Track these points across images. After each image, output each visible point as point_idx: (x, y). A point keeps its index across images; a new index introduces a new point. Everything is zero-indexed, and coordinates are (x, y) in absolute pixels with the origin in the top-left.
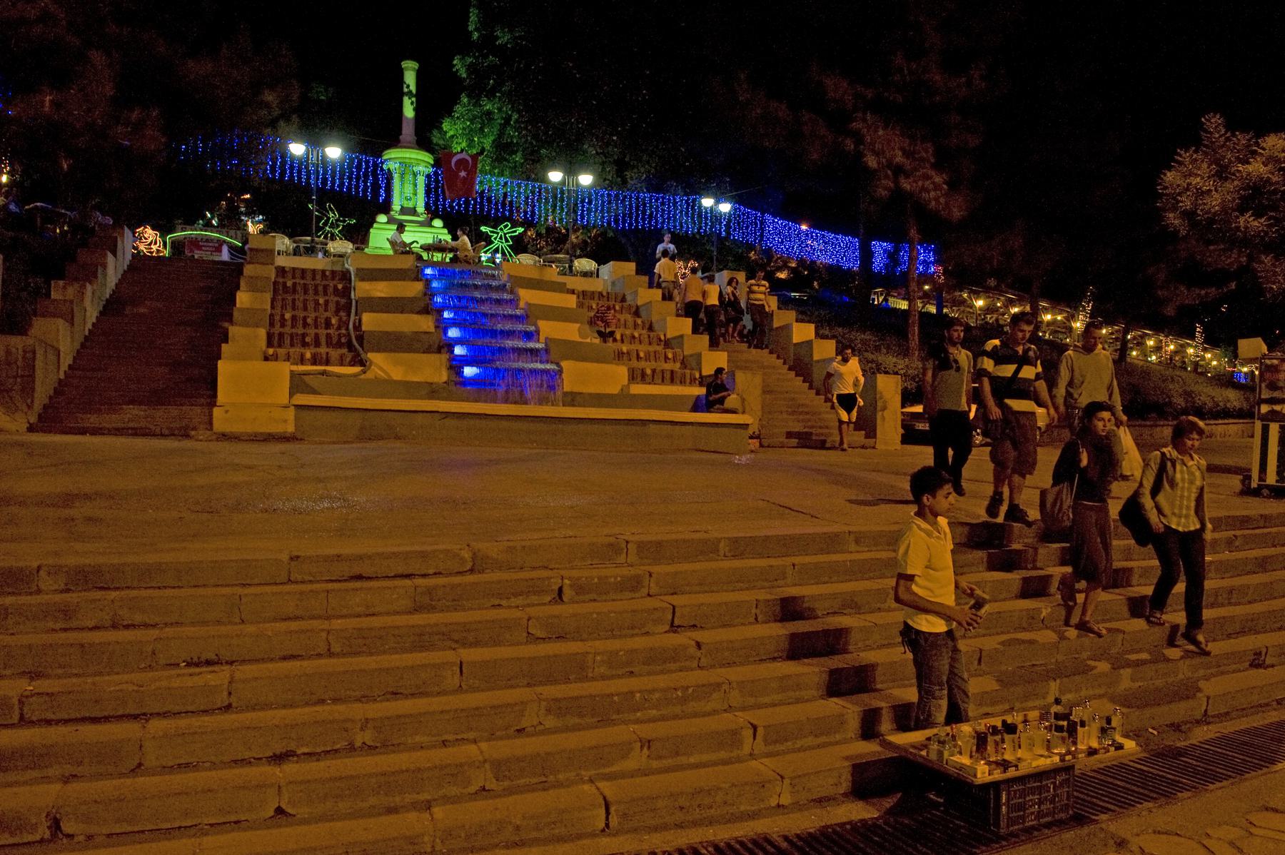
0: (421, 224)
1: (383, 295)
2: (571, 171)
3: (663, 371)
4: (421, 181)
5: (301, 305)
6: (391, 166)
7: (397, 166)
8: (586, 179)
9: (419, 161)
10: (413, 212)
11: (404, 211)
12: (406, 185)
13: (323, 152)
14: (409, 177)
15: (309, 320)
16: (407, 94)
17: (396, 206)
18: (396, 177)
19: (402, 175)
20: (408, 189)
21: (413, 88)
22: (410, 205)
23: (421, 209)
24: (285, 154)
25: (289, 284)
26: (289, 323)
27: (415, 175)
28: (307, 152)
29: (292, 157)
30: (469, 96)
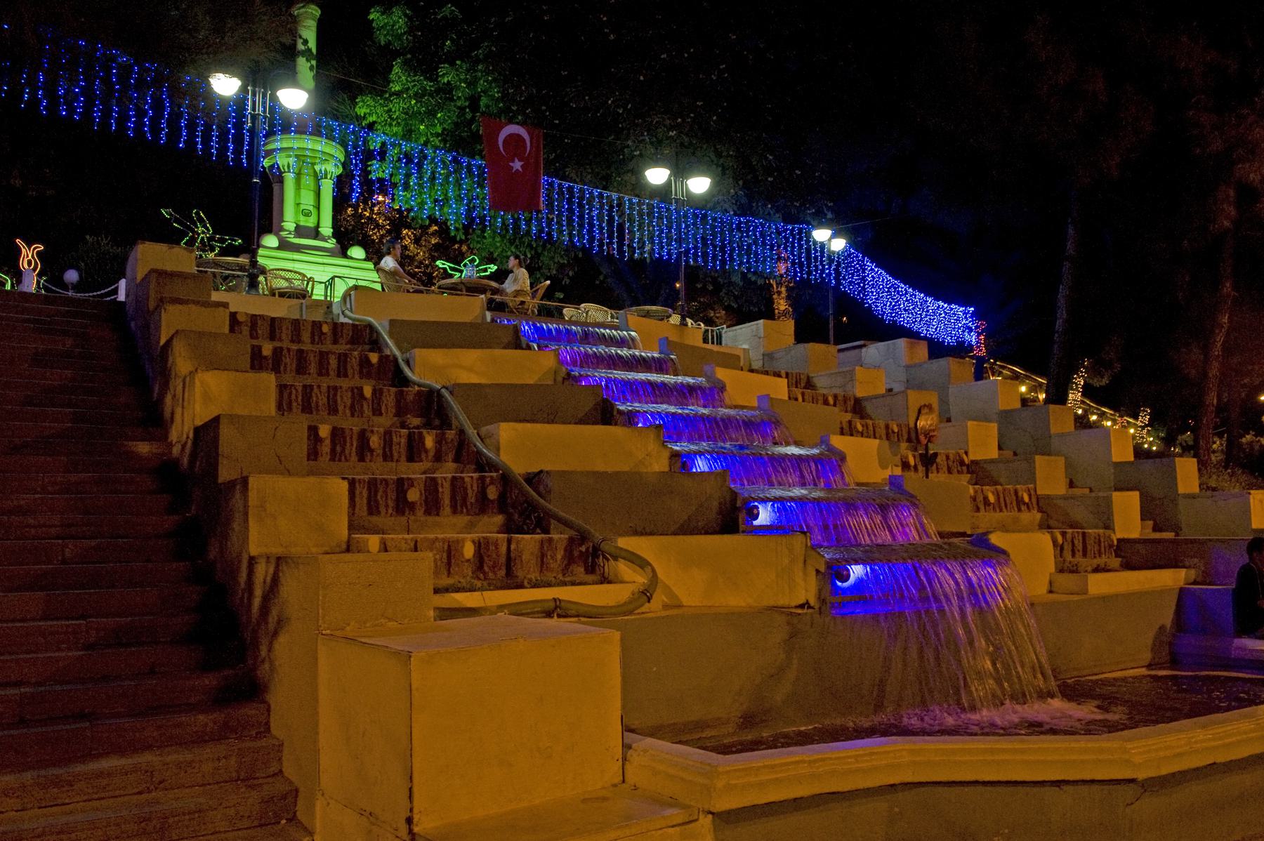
0: (331, 253)
1: (475, 379)
2: (681, 171)
3: (387, 457)
4: (328, 187)
5: (323, 400)
6: (282, 161)
7: (292, 160)
8: (699, 185)
9: (326, 157)
10: (315, 233)
11: (300, 231)
12: (303, 192)
13: (274, 99)
14: (308, 181)
15: (375, 441)
16: (303, 53)
17: (289, 225)
18: (289, 178)
19: (298, 175)
20: (308, 199)
21: (312, 45)
22: (310, 222)
23: (327, 230)
24: (208, 93)
25: (267, 349)
26: (326, 448)
27: (318, 178)
28: (244, 89)
29: (223, 101)
30: (409, 67)
